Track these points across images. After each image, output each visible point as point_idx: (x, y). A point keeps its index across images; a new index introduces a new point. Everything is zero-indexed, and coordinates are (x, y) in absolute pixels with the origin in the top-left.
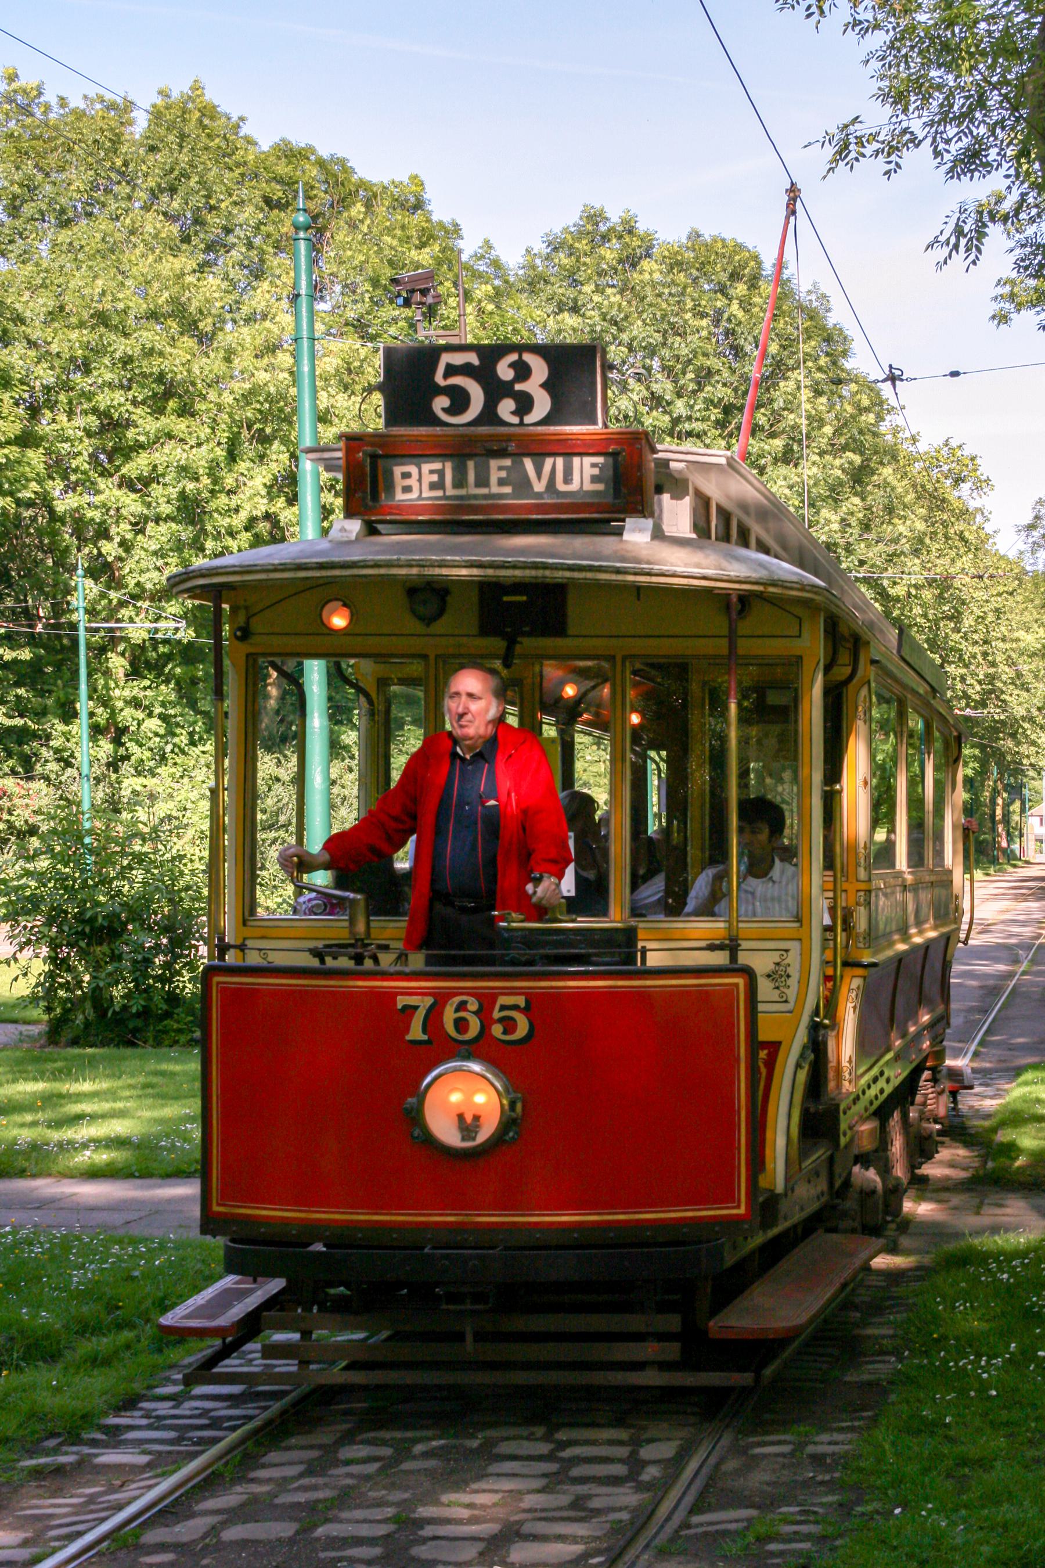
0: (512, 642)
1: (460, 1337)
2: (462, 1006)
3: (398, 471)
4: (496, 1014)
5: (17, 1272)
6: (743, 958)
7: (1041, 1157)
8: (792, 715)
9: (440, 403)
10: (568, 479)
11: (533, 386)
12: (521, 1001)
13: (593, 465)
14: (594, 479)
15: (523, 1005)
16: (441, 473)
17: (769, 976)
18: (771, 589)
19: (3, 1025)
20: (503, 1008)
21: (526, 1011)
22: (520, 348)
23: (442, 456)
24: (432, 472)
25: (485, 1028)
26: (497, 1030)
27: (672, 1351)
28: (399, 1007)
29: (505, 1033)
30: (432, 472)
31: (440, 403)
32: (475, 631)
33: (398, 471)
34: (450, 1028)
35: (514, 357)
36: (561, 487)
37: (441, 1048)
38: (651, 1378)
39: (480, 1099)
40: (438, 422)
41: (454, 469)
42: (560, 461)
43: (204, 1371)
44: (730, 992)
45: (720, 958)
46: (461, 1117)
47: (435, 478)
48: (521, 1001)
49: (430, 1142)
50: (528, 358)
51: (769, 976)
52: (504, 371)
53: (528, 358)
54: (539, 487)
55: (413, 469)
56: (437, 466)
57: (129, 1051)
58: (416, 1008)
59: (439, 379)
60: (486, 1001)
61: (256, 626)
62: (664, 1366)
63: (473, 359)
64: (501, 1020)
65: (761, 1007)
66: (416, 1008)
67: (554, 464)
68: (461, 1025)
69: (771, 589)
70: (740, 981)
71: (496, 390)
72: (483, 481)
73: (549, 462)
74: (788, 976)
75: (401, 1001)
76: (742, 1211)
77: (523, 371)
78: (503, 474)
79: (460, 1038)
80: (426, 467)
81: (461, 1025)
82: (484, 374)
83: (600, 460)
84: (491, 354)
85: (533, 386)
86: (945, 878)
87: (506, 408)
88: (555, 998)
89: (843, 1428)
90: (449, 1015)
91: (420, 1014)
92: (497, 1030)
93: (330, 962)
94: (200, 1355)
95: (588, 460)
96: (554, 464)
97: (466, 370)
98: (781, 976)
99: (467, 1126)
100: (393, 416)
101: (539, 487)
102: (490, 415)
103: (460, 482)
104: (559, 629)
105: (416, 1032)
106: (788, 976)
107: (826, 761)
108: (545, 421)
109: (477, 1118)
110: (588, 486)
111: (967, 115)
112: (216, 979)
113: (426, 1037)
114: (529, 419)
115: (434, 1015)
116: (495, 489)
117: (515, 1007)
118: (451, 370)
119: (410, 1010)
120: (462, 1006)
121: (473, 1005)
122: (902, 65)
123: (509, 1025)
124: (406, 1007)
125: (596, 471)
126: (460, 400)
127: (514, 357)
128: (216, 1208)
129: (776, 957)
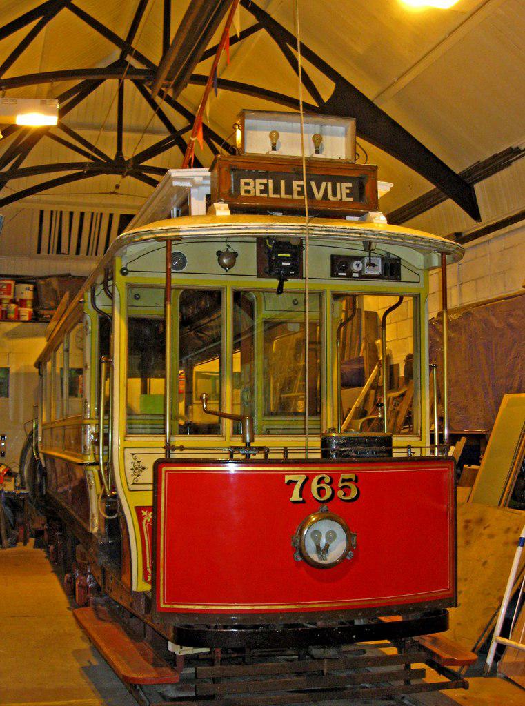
3: (243, 181)
10: (334, 194)
12: (353, 477)
14: (348, 195)
15: (354, 479)
16: (266, 185)
17: (144, 468)
20: (344, 481)
24: (347, 188)
26: (340, 494)
28: (286, 481)
29: (344, 495)
30: (261, 184)
33: (243, 181)
37: (307, 505)
44: (172, 477)
48: (353, 477)
51: (144, 468)
54: (319, 196)
55: (251, 181)
56: (265, 181)
58: (296, 482)
64: (343, 488)
66: (296, 482)
67: (326, 186)
68: (321, 491)
70: (164, 469)
72: (289, 190)
74: (132, 469)
76: (162, 606)
79: (322, 499)
80: (258, 181)
83: (350, 185)
90: (314, 486)
92: (340, 494)
95: (345, 185)
96: (326, 186)
98: (136, 469)
101: (319, 196)
103: (277, 190)
105: (296, 496)
106: (132, 469)
113: (301, 499)
115: (307, 482)
117: (349, 480)
120: (320, 481)
121: (328, 480)
124: (290, 482)
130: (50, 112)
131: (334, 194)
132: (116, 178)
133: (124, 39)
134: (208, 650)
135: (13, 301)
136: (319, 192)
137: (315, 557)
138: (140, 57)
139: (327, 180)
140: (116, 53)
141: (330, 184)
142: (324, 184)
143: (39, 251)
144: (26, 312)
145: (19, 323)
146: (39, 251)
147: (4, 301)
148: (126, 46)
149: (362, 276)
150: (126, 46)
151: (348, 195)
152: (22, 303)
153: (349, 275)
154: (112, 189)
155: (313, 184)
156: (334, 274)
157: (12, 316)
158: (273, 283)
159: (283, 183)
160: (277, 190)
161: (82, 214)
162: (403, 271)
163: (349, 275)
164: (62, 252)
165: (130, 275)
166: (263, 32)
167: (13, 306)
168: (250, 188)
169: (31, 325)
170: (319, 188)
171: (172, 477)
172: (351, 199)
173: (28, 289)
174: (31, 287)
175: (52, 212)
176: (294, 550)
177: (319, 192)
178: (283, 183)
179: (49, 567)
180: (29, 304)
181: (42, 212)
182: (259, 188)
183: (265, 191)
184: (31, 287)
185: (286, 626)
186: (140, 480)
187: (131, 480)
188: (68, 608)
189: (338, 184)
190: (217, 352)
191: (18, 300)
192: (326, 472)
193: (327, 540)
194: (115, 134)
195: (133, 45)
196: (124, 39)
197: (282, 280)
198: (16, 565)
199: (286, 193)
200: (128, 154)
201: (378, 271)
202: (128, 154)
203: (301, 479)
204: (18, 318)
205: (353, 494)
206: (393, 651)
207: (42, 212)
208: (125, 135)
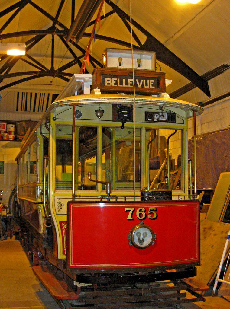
3: (106, 79)
10: (147, 85)
12: (154, 209)
14: (152, 85)
15: (155, 210)
16: (117, 81)
17: (63, 205)
20: (151, 210)
24: (152, 82)
26: (149, 216)
28: (125, 211)
29: (151, 217)
30: (114, 81)
33: (106, 79)
37: (135, 221)
43: (66, 304)
44: (75, 209)
47: (115, 82)
48: (154, 209)
51: (63, 205)
54: (140, 86)
55: (110, 79)
56: (116, 79)
58: (130, 211)
64: (150, 213)
66: (130, 211)
67: (143, 82)
68: (141, 215)
70: (72, 205)
72: (127, 83)
74: (58, 205)
76: (71, 265)
79: (141, 218)
80: (113, 79)
83: (153, 81)
90: (138, 213)
92: (149, 216)
95: (151, 81)
96: (143, 82)
98: (60, 205)
101: (140, 86)
103: (121, 83)
105: (130, 217)
106: (58, 205)
113: (132, 218)
115: (134, 211)
117: (153, 210)
120: (140, 210)
121: (143, 210)
123: (152, 214)
124: (127, 211)
129: (61, 210)
130: (22, 49)
131: (147, 85)
132: (51, 78)
133: (55, 17)
135: (6, 132)
136: (140, 84)
137: (138, 244)
138: (61, 25)
139: (143, 79)
140: (51, 23)
141: (144, 81)
142: (142, 81)
143: (17, 110)
144: (11, 136)
145: (8, 142)
146: (17, 110)
147: (2, 132)
148: (55, 20)
149: (159, 121)
150: (55, 20)
151: (152, 85)
152: (10, 133)
153: (153, 120)
154: (49, 83)
155: (137, 81)
156: (146, 120)
157: (5, 138)
158: (120, 124)
159: (124, 80)
160: (121, 83)
161: (36, 94)
162: (177, 118)
163: (153, 120)
164: (27, 110)
165: (57, 120)
166: (115, 14)
167: (6, 134)
168: (110, 82)
169: (13, 142)
170: (140, 82)
171: (75, 209)
172: (154, 87)
173: (12, 126)
174: (14, 125)
175: (23, 93)
176: (129, 241)
177: (140, 84)
178: (124, 80)
179: (21, 248)
180: (13, 133)
181: (18, 93)
182: (114, 82)
183: (116, 84)
184: (14, 125)
185: (125, 274)
186: (61, 210)
187: (57, 210)
188: (30, 266)
189: (148, 81)
190: (95, 154)
191: (8, 131)
192: (143, 206)
193: (143, 236)
194: (50, 59)
195: (58, 20)
196: (55, 17)
197: (124, 122)
198: (7, 247)
199: (125, 85)
200: (56, 68)
201: (165, 119)
202: (56, 68)
203: (132, 210)
204: (8, 139)
205: (155, 216)
206: (172, 285)
207: (18, 93)
208: (55, 59)
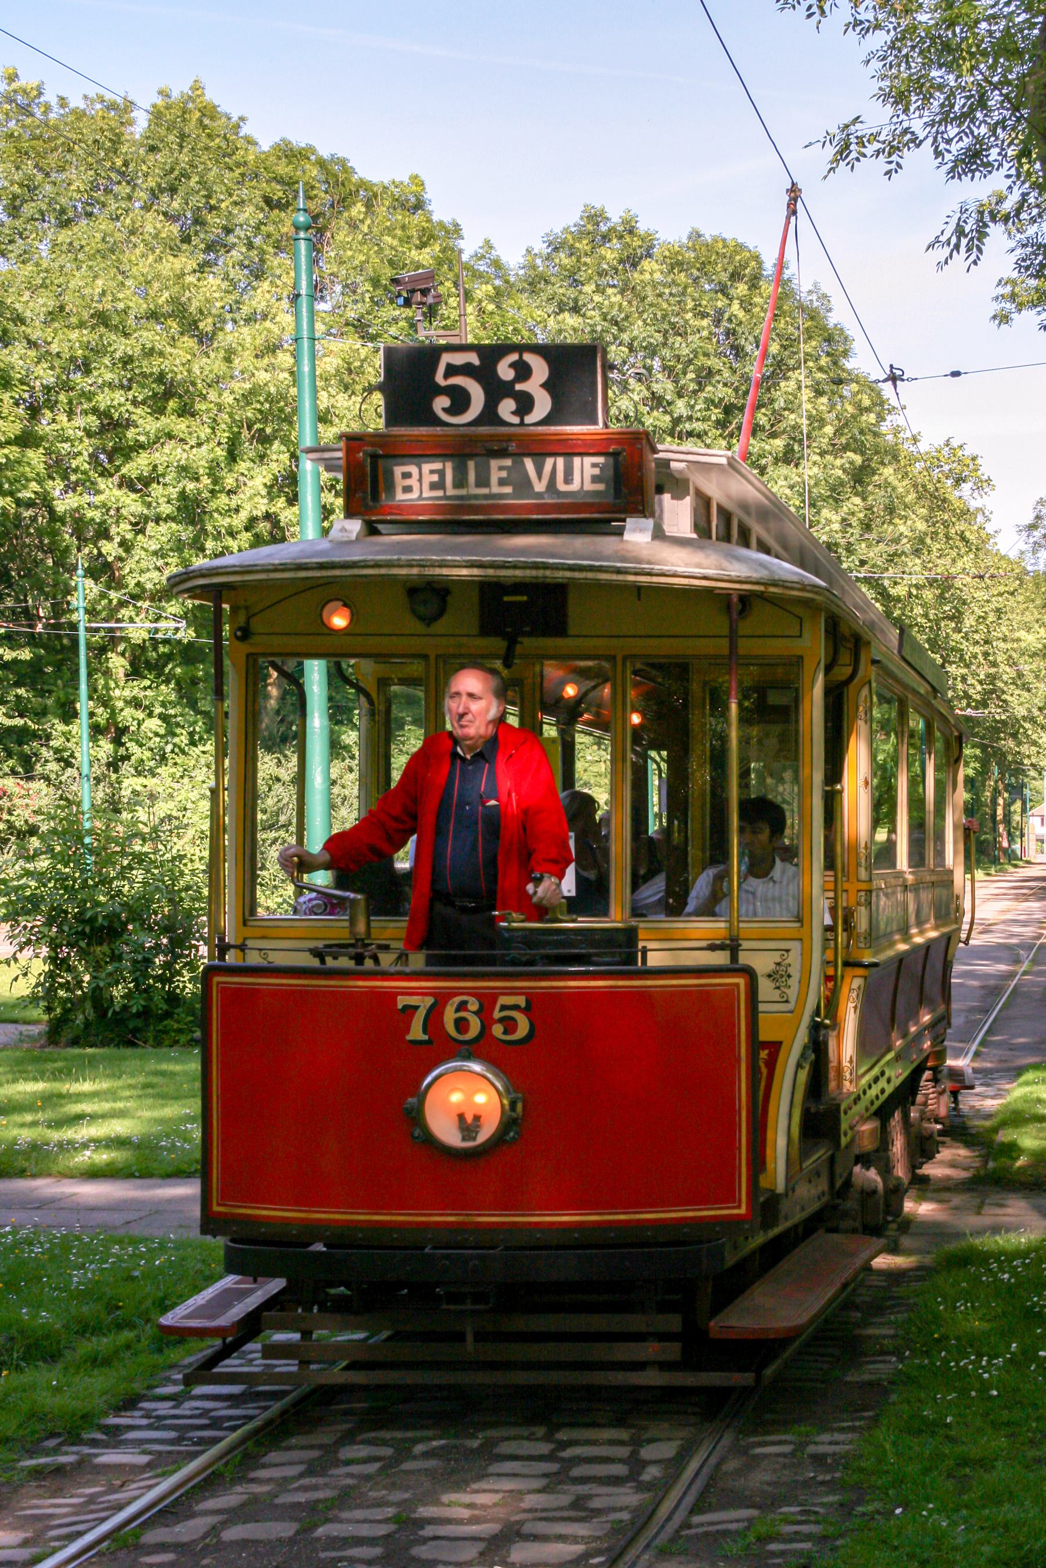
0: (512, 642)
1: (461, 1337)
2: (462, 1006)
3: (398, 471)
4: (497, 1014)
5: (17, 1272)
6: (744, 958)
7: (1042, 1157)
8: (793, 715)
9: (441, 403)
10: (568, 479)
11: (534, 386)
12: (521, 1001)
13: (594, 465)
14: (595, 479)
15: (523, 1005)
16: (442, 473)
17: (769, 976)
18: (772, 589)
19: (3, 1025)
20: (504, 1008)
21: (527, 1011)
22: (521, 348)
23: (443, 456)
24: (432, 472)
25: (486, 1028)
26: (497, 1030)
27: (673, 1351)
28: (400, 1007)
29: (505, 1033)
30: (432, 472)
31: (441, 403)
32: (475, 631)
33: (398, 471)
34: (450, 1028)
35: (514, 357)
36: (562, 487)
37: (441, 1048)
38: (652, 1378)
39: (480, 1099)
40: (438, 422)
41: (455, 469)
42: (560, 461)
44: (731, 992)
45: (720, 958)
46: (461, 1117)
47: (435, 478)
48: (521, 1001)
49: (430, 1142)
50: (529, 358)
51: (769, 976)
52: (505, 371)
53: (529, 358)
55: (413, 469)
56: (438, 466)
57: (129, 1051)
58: (417, 1008)
59: (439, 379)
60: (487, 1001)
61: (257, 626)
62: (664, 1366)
63: (473, 359)
64: (502, 1020)
65: (762, 1007)
66: (417, 1008)
67: (555, 464)
68: (461, 1025)
69: (772, 589)
71: (496, 390)
72: (483, 481)
73: (549, 462)
74: (789, 976)
75: (402, 1001)
76: (743, 1211)
77: (523, 371)
78: (504, 474)
79: (461, 1038)
80: (427, 467)
81: (461, 1025)
82: (485, 374)
83: (601, 460)
84: (491, 354)
85: (534, 386)
86: (946, 878)
87: (506, 408)
88: (556, 998)
89: (844, 1428)
90: (450, 1015)
91: (421, 1014)
92: (497, 1030)
93: (330, 962)
94: (200, 1355)
95: (588, 460)
96: (555, 464)
97: (466, 370)
98: (782, 976)
99: (468, 1126)
100: (394, 416)
101: (540, 487)
102: (490, 415)
103: (460, 482)
104: (559, 629)
105: (416, 1032)
106: (789, 976)
107: (827, 761)
108: (545, 421)
109: (477, 1118)
110: (589, 486)
111: (968, 115)
112: (216, 979)
113: (426, 1037)
114: (529, 419)
115: (434, 1015)
116: (495, 489)
117: (516, 1007)
118: (452, 370)
119: (411, 1010)
120: (462, 1006)
121: (474, 1005)
122: (903, 65)
123: (510, 1025)
124: (406, 1007)
125: (597, 471)
126: (460, 400)
127: (514, 357)
128: (216, 1208)
129: (776, 957)
134: (296, 1336)
165: (255, 639)
206: (886, 1342)
